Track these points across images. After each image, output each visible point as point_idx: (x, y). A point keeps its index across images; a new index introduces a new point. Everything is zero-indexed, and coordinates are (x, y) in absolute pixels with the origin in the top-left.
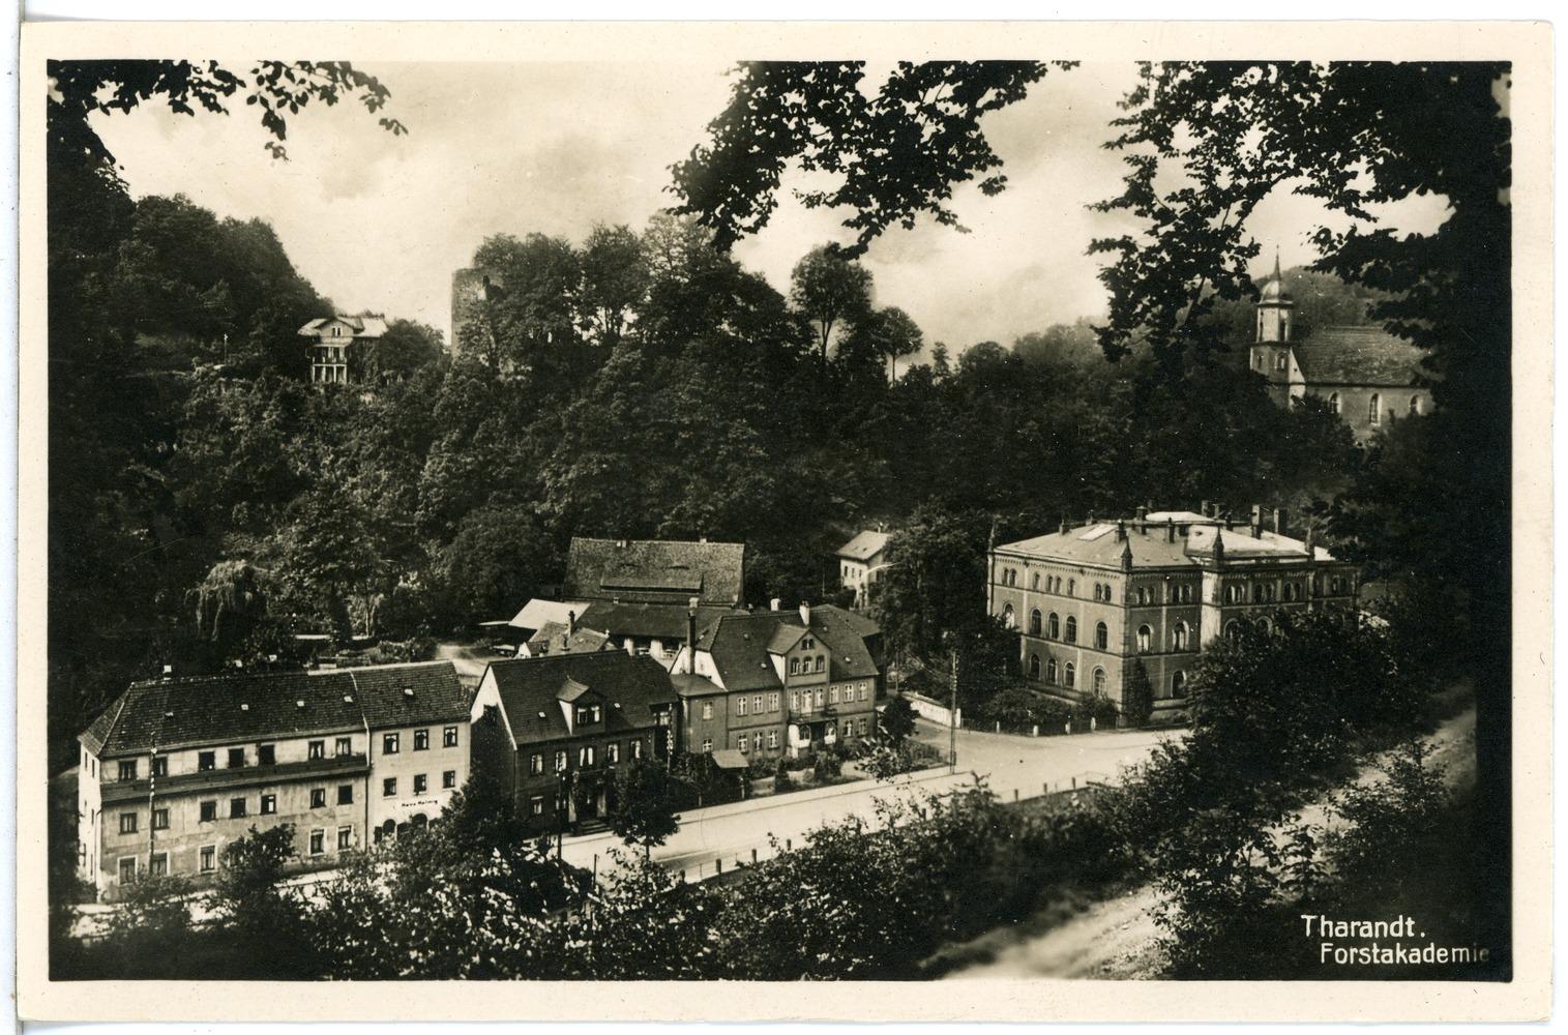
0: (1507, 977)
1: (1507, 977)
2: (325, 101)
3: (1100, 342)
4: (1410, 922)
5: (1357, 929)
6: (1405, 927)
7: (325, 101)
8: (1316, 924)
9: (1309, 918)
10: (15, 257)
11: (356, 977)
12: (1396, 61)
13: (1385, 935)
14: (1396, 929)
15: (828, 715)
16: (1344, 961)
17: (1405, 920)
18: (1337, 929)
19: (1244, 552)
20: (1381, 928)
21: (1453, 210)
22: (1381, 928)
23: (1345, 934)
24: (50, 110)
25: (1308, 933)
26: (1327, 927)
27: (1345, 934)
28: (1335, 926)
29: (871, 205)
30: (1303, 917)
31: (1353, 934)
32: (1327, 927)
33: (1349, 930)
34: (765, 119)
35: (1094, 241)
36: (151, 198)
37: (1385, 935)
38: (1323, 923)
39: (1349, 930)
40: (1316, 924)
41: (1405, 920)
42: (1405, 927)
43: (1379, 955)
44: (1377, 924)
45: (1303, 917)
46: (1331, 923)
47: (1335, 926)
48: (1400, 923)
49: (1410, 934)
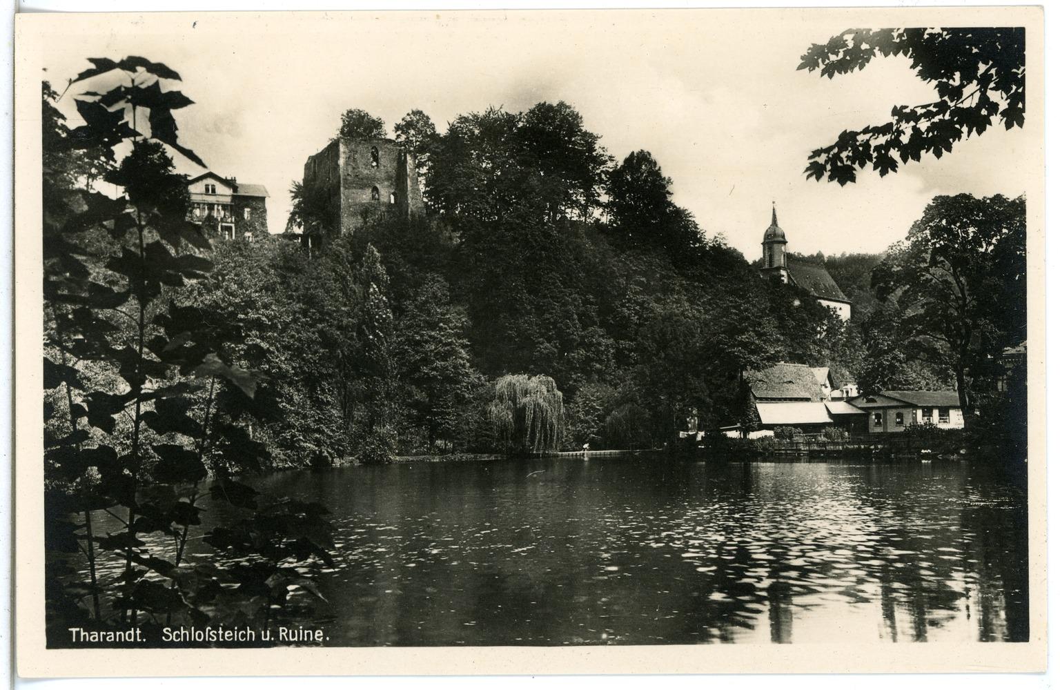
0: (1021, 31)
2: (826, 75)
5: (105, 637)
6: (135, 634)
7: (826, 75)
8: (78, 633)
9: (74, 630)
10: (10, 212)
11: (47, 616)
12: (680, 198)
14: (130, 636)
16: (201, 640)
17: (135, 631)
18: (92, 637)
19: (10, 467)
22: (120, 635)
23: (97, 640)
24: (919, 29)
25: (74, 640)
26: (85, 636)
27: (97, 640)
28: (90, 635)
30: (70, 629)
31: (117, 640)
32: (85, 636)
33: (99, 638)
36: (306, 165)
38: (82, 634)
39: (99, 638)
40: (78, 633)
42: (135, 634)
43: (223, 635)
45: (70, 629)
46: (87, 634)
47: (90, 635)
48: (132, 632)
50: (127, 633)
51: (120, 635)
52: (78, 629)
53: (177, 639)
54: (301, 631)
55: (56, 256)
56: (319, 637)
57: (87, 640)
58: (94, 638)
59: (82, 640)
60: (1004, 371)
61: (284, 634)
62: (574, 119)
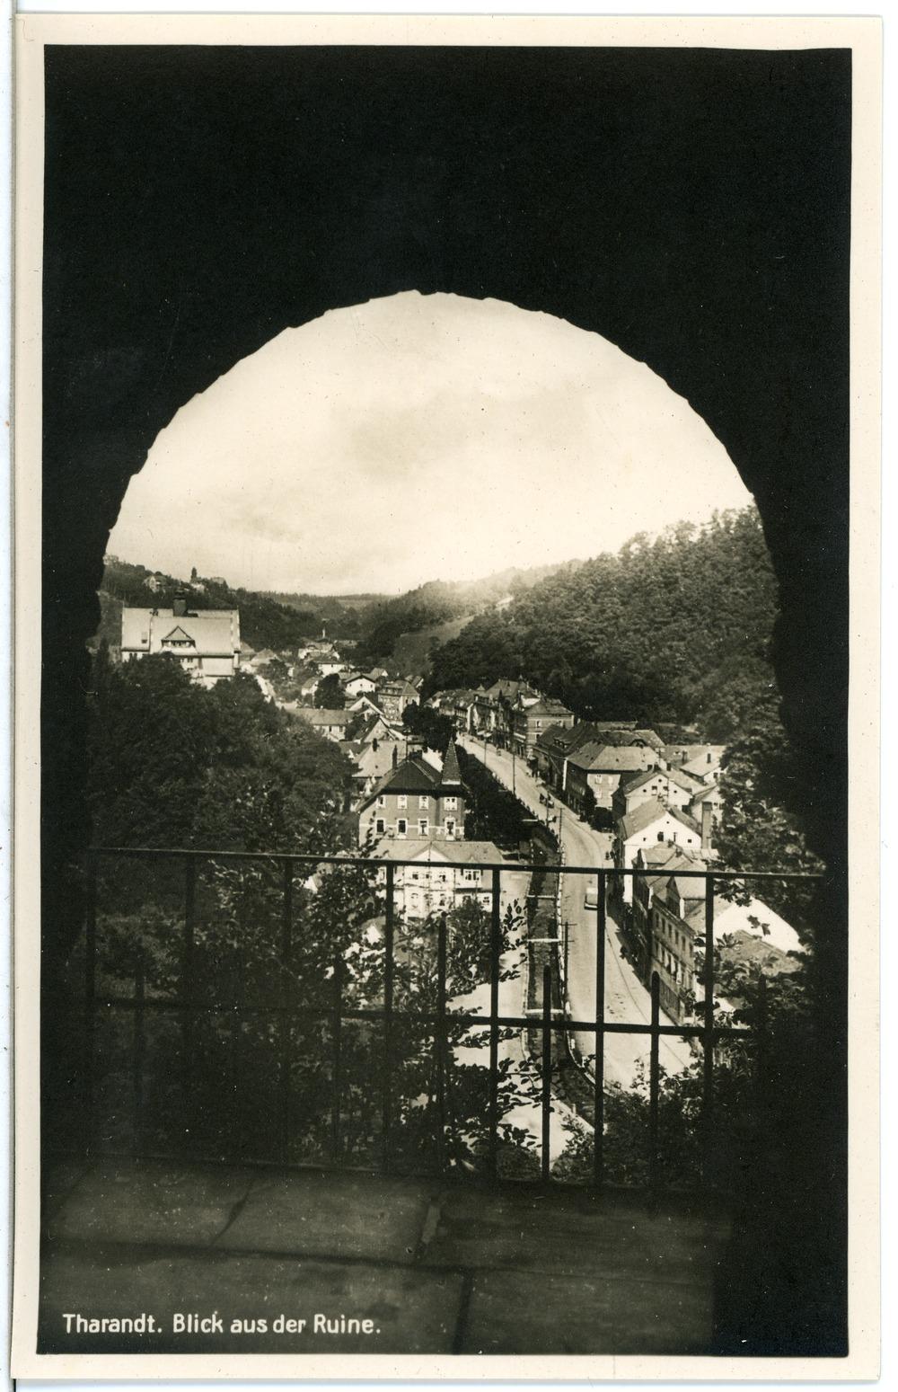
0: (45, 46)
1: (45, 46)
3: (722, 807)
4: (151, 1320)
5: (107, 1325)
6: (147, 1323)
8: (74, 1321)
9: (69, 1317)
13: (130, 1330)
15: (654, 636)
17: (147, 1317)
18: (91, 1326)
20: (127, 1324)
21: (502, 957)
22: (127, 1324)
26: (82, 1324)
28: (89, 1323)
29: (557, 938)
30: (65, 1316)
31: (350, 1331)
32: (82, 1324)
34: (320, 920)
35: (768, 925)
37: (130, 1330)
38: (80, 1320)
41: (147, 1317)
42: (147, 1323)
44: (124, 1321)
45: (65, 1316)
47: (89, 1323)
48: (143, 1321)
49: (151, 1330)
50: (137, 1322)
51: (354, 1325)
52: (74, 1316)
53: (206, 1328)
54: (343, 1322)
55: (522, 823)
56: (368, 1329)
57: (86, 1330)
58: (94, 1328)
59: (69, 1330)
60: (413, 975)
61: (322, 1324)
62: (592, 566)
